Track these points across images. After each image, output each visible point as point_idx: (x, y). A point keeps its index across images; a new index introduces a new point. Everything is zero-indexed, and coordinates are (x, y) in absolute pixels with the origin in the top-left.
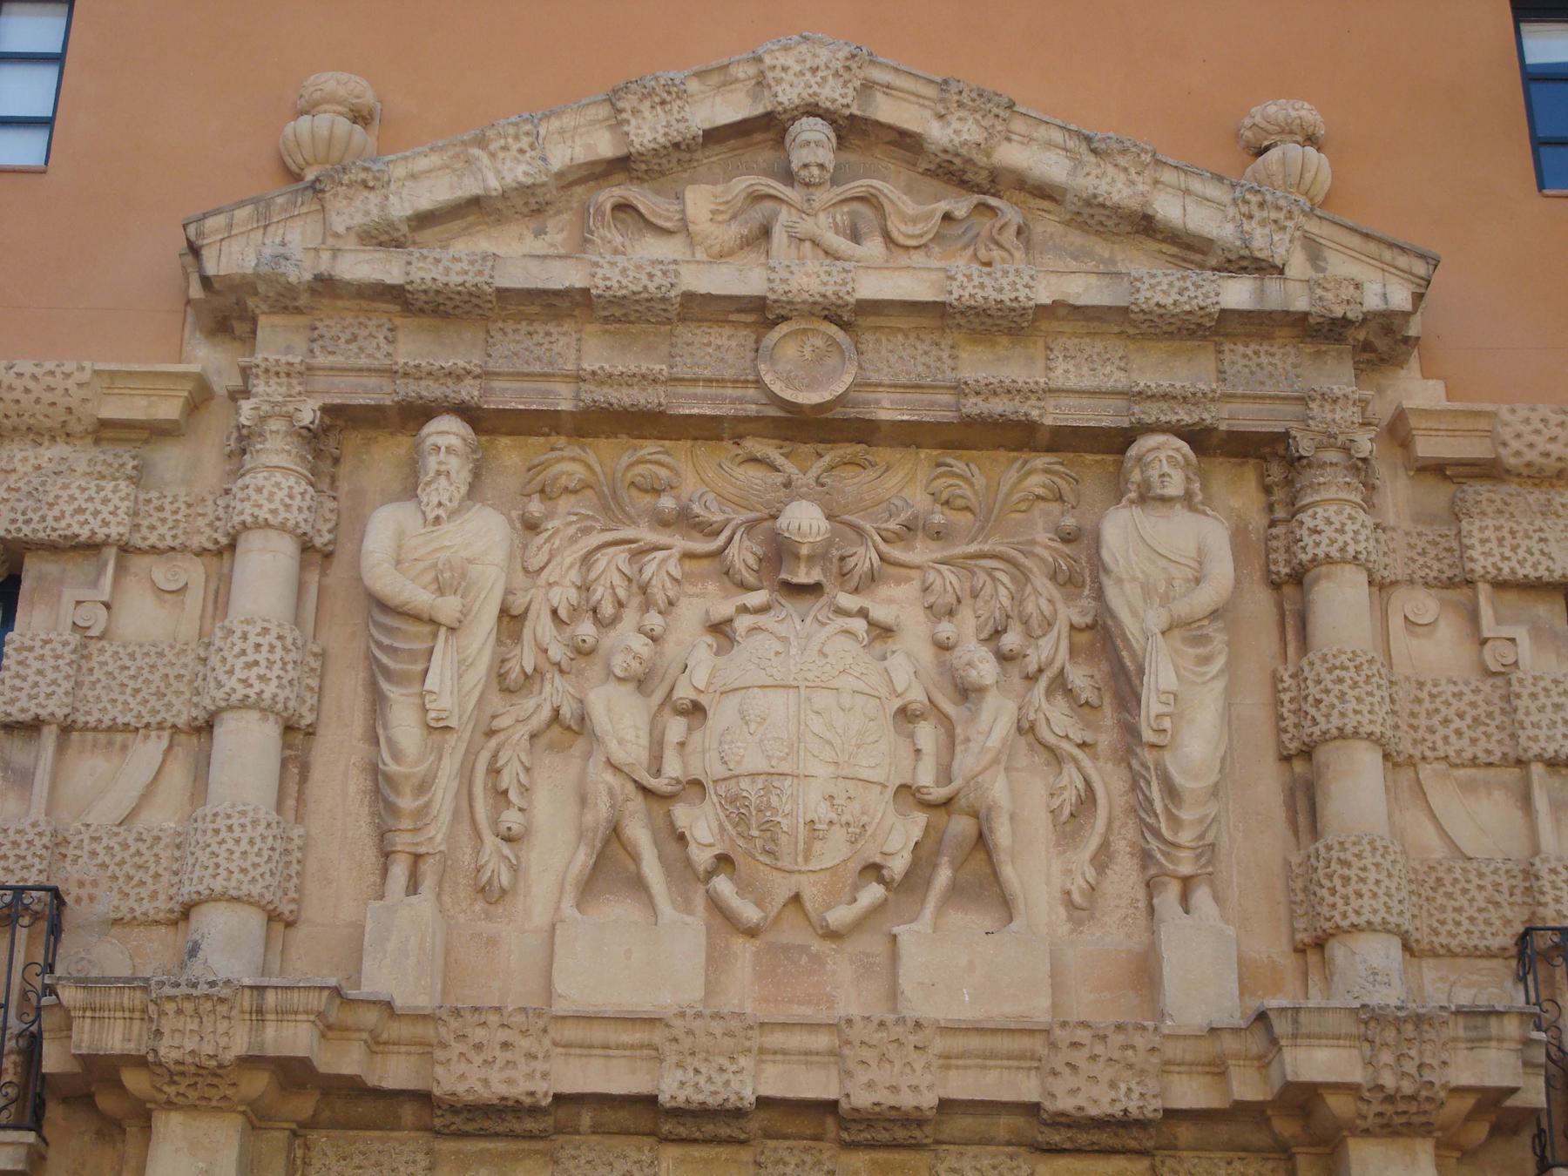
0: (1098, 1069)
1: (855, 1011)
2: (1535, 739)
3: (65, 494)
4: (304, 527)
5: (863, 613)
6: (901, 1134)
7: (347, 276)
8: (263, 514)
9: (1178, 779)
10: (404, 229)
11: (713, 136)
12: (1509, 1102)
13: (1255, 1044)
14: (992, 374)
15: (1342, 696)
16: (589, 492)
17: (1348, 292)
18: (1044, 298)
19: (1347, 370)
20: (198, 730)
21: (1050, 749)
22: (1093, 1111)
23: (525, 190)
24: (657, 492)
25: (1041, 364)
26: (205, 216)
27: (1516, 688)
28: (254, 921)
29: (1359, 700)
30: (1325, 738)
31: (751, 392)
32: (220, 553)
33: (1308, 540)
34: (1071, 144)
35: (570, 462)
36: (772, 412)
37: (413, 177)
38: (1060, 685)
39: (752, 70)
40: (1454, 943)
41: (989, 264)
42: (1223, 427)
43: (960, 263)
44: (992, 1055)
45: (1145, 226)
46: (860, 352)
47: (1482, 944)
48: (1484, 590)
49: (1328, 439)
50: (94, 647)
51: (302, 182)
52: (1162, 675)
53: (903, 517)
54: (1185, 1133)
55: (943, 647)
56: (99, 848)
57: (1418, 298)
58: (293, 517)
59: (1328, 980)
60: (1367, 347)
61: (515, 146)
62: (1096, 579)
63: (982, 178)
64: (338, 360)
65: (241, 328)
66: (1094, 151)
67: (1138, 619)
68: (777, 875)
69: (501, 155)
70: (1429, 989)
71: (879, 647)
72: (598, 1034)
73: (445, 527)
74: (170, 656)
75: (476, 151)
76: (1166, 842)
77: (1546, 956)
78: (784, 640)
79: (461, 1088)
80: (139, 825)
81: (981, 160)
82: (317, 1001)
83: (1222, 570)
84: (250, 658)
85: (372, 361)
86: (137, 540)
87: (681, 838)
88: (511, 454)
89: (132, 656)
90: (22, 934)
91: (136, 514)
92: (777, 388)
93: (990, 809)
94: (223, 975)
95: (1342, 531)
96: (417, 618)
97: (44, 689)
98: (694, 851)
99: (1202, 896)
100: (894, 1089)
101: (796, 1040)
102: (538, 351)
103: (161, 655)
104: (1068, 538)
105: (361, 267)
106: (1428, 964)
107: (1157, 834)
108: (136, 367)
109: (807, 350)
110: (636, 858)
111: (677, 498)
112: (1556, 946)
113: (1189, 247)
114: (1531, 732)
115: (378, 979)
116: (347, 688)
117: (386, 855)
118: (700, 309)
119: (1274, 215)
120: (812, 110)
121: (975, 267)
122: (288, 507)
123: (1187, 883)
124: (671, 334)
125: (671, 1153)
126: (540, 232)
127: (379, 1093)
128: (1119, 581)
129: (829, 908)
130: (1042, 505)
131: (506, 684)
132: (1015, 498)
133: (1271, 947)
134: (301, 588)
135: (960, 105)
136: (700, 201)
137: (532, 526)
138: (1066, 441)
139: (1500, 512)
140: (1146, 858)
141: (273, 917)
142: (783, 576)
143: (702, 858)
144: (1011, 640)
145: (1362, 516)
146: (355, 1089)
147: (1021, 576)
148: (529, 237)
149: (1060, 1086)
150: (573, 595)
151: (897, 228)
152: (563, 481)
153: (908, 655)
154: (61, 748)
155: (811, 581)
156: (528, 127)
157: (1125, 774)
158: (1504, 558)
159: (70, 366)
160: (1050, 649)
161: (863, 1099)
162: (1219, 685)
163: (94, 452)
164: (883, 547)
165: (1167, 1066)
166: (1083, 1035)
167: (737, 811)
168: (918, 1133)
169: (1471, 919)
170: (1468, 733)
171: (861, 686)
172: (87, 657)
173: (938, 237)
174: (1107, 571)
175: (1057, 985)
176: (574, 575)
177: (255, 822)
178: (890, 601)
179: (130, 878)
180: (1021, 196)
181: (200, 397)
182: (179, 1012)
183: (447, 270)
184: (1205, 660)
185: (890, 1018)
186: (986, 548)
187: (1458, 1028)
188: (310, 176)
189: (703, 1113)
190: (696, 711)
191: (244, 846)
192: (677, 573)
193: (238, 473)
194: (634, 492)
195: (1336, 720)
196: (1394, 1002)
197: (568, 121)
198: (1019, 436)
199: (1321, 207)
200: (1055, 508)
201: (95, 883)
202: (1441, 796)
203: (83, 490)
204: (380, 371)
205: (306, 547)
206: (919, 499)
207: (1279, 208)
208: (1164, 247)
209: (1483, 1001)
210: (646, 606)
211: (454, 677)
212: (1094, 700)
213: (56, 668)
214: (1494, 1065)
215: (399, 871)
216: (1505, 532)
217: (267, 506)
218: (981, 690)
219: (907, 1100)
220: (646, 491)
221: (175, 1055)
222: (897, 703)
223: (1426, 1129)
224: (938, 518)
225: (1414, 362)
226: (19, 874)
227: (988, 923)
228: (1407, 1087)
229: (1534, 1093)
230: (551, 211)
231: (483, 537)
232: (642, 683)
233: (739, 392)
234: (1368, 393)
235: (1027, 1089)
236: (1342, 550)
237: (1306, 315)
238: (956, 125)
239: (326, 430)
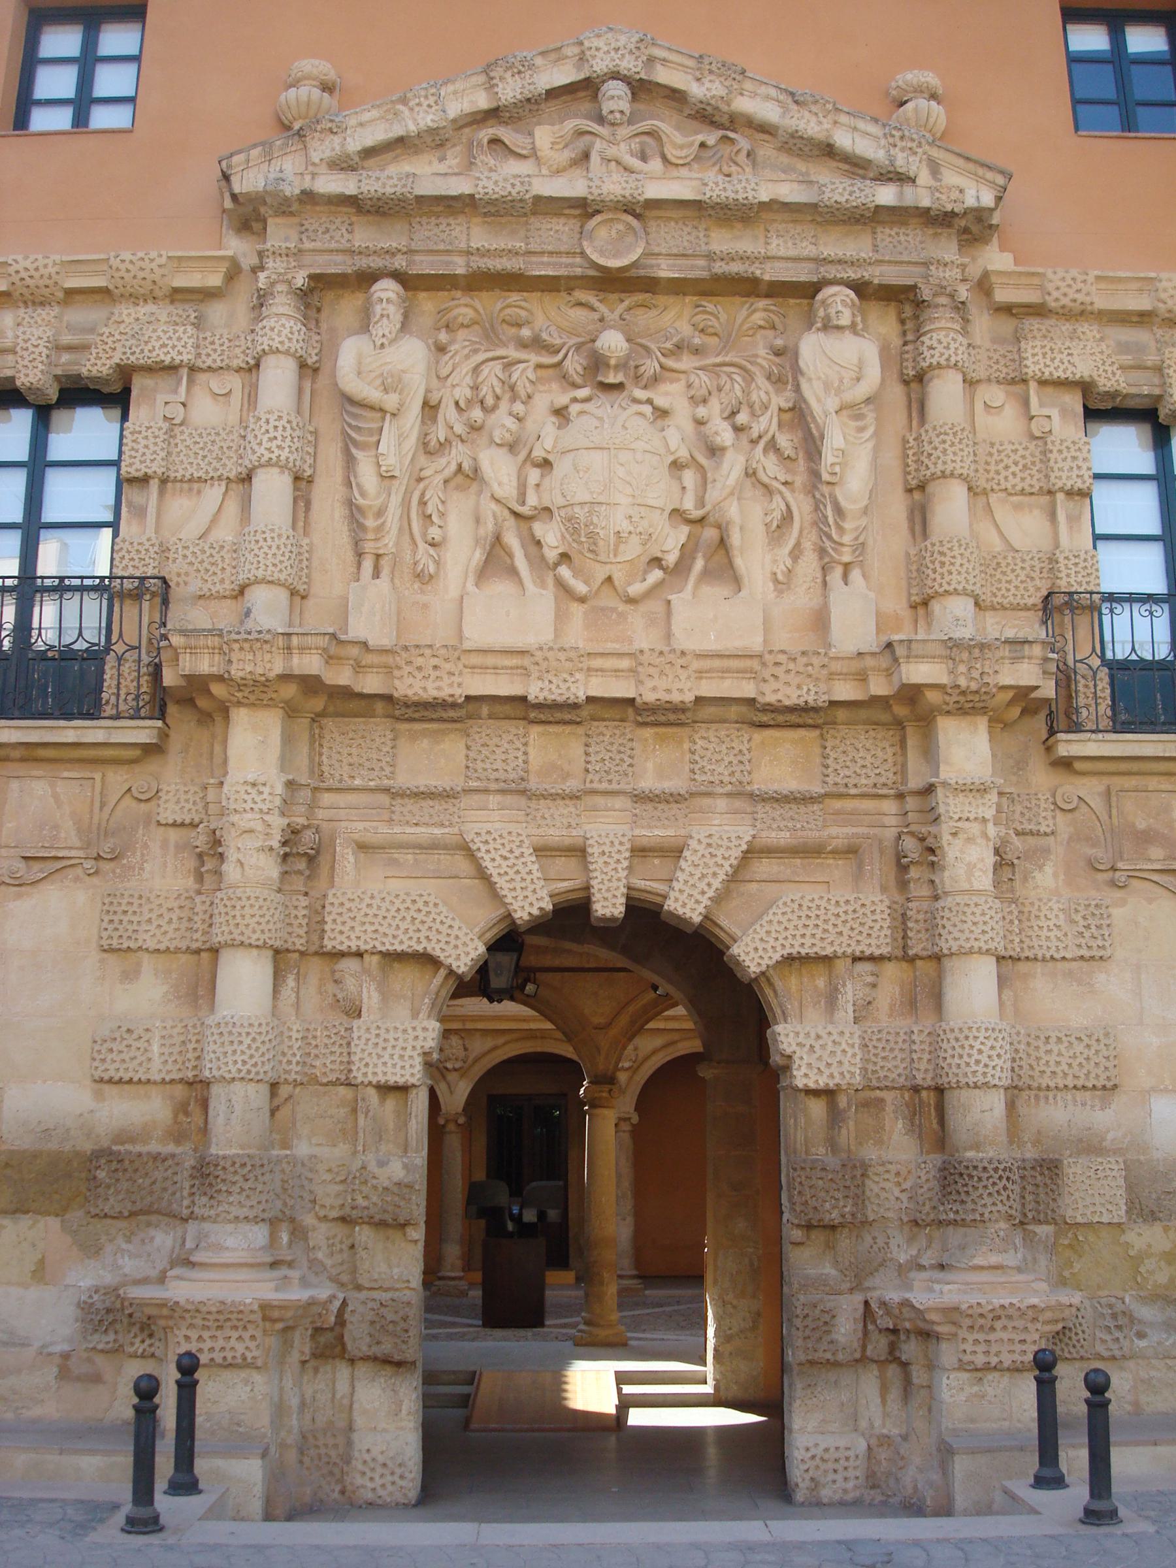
0: (790, 677)
1: (645, 646)
2: (1060, 478)
3: (154, 336)
4: (300, 352)
5: (649, 401)
6: (672, 717)
7: (321, 191)
8: (275, 345)
9: (843, 503)
10: (357, 159)
11: (552, 94)
12: (1033, 695)
13: (885, 661)
14: (732, 247)
15: (944, 451)
16: (476, 327)
17: (955, 195)
18: (764, 198)
19: (954, 246)
20: (243, 480)
21: (765, 486)
22: (787, 703)
23: (432, 131)
24: (519, 326)
25: (762, 240)
26: (232, 155)
27: (1050, 446)
28: (283, 595)
29: (955, 454)
30: (934, 477)
31: (578, 260)
32: (250, 370)
33: (927, 354)
34: (781, 97)
35: (464, 307)
36: (592, 273)
37: (361, 125)
38: (772, 446)
39: (576, 50)
40: (1005, 602)
41: (729, 176)
42: (876, 281)
43: (711, 175)
44: (728, 671)
45: (828, 151)
46: (647, 234)
47: (1022, 602)
48: (1033, 385)
49: (941, 290)
50: (177, 430)
51: (292, 130)
52: (835, 438)
53: (675, 340)
54: (841, 714)
55: (700, 423)
56: (188, 553)
57: (999, 199)
58: (294, 346)
59: (929, 624)
60: (966, 231)
61: (425, 103)
62: (795, 379)
63: (725, 120)
64: (318, 245)
65: (256, 226)
66: (796, 102)
67: (821, 403)
68: (598, 565)
69: (417, 109)
70: (989, 629)
71: (659, 423)
72: (490, 660)
73: (387, 350)
74: (223, 434)
75: (400, 107)
76: (835, 542)
77: (1059, 610)
78: (600, 419)
79: (410, 693)
80: (211, 538)
81: (725, 108)
82: (323, 642)
83: (874, 373)
84: (272, 435)
85: (338, 245)
86: (199, 363)
87: (539, 543)
88: (427, 303)
89: (201, 435)
90: (146, 605)
91: (198, 347)
92: (594, 257)
93: (728, 523)
94: (266, 627)
95: (947, 348)
96: (372, 408)
97: (149, 457)
98: (546, 550)
99: (856, 574)
100: (668, 691)
101: (609, 663)
102: (443, 236)
103: (218, 434)
104: (778, 353)
105: (331, 184)
106: (989, 614)
107: (830, 537)
108: (193, 254)
109: (614, 232)
110: (510, 555)
111: (532, 329)
112: (1066, 603)
113: (855, 165)
114: (1057, 474)
115: (358, 629)
116: (331, 453)
117: (360, 555)
118: (545, 206)
119: (909, 145)
120: (615, 76)
121: (720, 178)
122: (290, 339)
123: (847, 567)
124: (527, 223)
125: (535, 730)
126: (442, 159)
127: (361, 696)
128: (810, 380)
129: (629, 584)
130: (763, 332)
131: (429, 448)
132: (745, 327)
133: (896, 604)
134: (300, 391)
135: (711, 72)
136: (544, 136)
138: (779, 290)
139: (1045, 337)
140: (822, 552)
141: (293, 593)
142: (600, 378)
143: (551, 555)
144: (742, 418)
145: (960, 338)
146: (347, 693)
147: (749, 377)
148: (435, 162)
149: (767, 688)
150: (468, 393)
151: (670, 152)
152: (460, 320)
153: (678, 427)
154: (162, 493)
155: (616, 381)
156: (433, 90)
157: (811, 501)
158: (1047, 366)
159: (153, 254)
160: (766, 423)
161: (650, 697)
162: (870, 445)
163: (171, 308)
164: (662, 359)
165: (831, 676)
166: (782, 658)
167: (572, 526)
168: (682, 717)
169: (1016, 587)
170: (1020, 475)
171: (648, 447)
172: (174, 437)
173: (697, 158)
174: (802, 374)
175: (767, 631)
176: (468, 380)
177: (280, 536)
178: (667, 394)
179: (207, 570)
180: (748, 132)
181: (233, 272)
182: (241, 649)
183: (384, 185)
184: (861, 429)
185: (666, 649)
186: (727, 359)
187: (1006, 651)
188: (296, 126)
189: (555, 706)
190: (546, 464)
191: (274, 550)
192: (532, 377)
193: (259, 319)
194: (505, 326)
195: (940, 467)
196: (968, 636)
197: (459, 85)
198: (748, 287)
199: (941, 140)
200: (770, 333)
201: (187, 574)
202: (1002, 513)
203: (165, 332)
204: (344, 251)
205: (303, 365)
206: (685, 329)
207: (913, 140)
208: (841, 165)
209: (1021, 635)
210: (514, 399)
211: (396, 444)
212: (793, 455)
213: (156, 444)
214: (1026, 673)
215: (368, 564)
216: (1047, 349)
217: (277, 339)
218: (723, 449)
219: (676, 697)
220: (512, 325)
221: (241, 674)
222: (671, 458)
223: (984, 710)
224: (697, 341)
225: (995, 240)
226: (142, 569)
227: (726, 593)
228: (974, 686)
229: (1048, 690)
230: (449, 145)
231: (410, 356)
232: (512, 447)
233: (570, 260)
234: (966, 260)
235: (747, 690)
236: (948, 360)
237: (929, 209)
238: (708, 85)
239: (312, 290)
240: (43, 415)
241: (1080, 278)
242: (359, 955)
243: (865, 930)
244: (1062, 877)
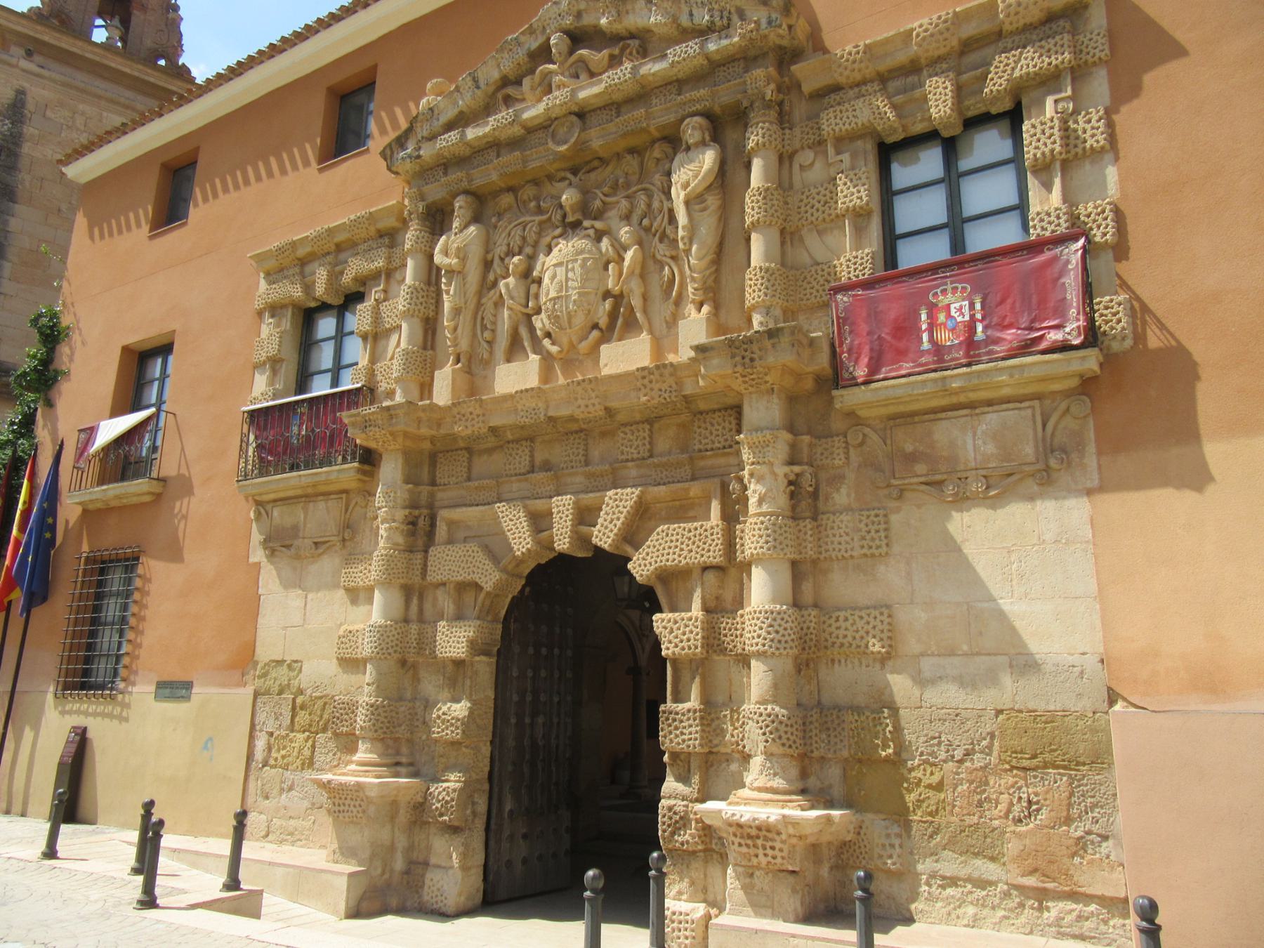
240: (951, 148)
242: (444, 584)
243: (706, 547)
244: (853, 495)
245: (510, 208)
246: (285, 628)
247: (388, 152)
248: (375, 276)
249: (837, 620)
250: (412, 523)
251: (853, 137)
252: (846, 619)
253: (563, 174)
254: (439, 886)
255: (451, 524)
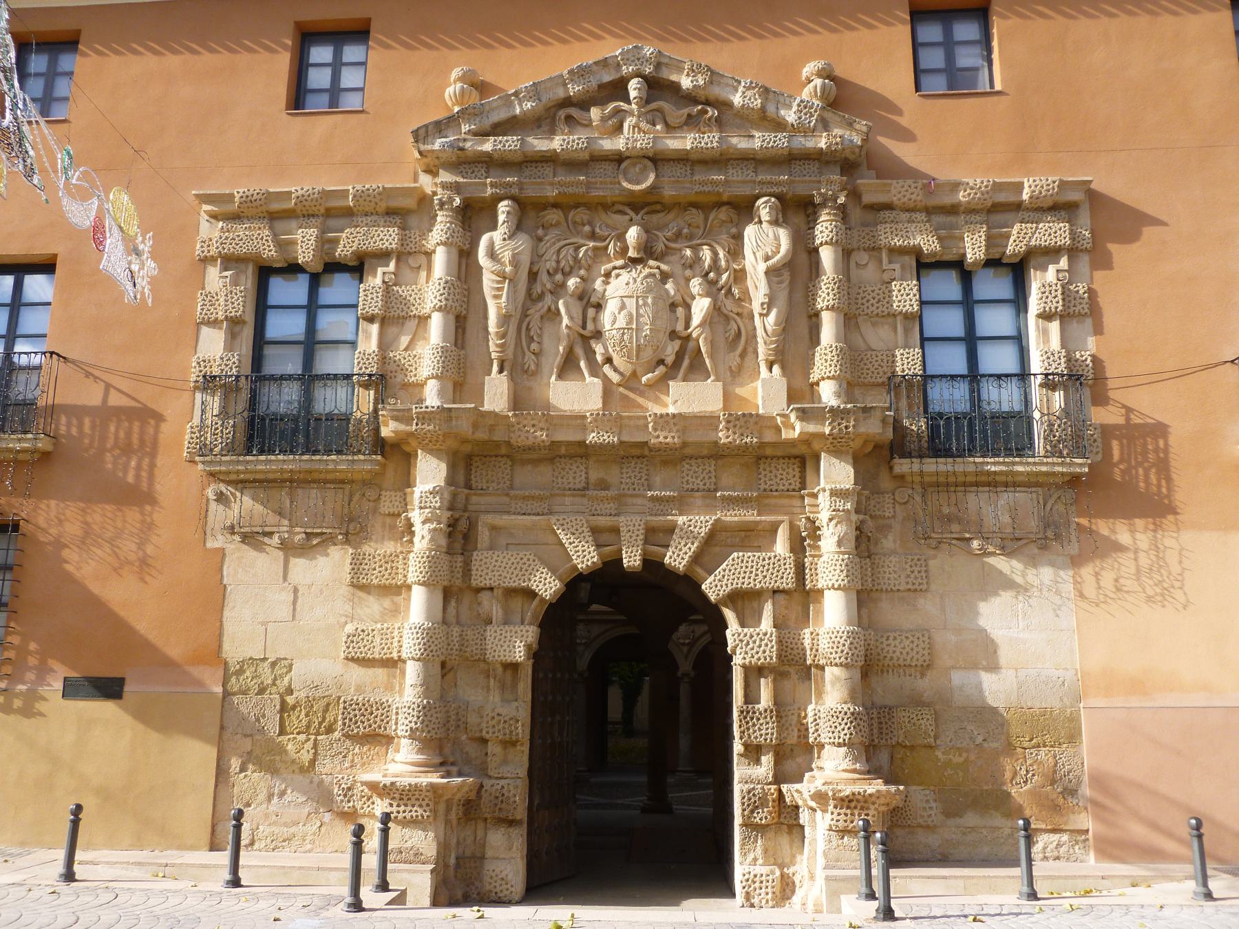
5: (658, 268)
136: (595, 113)
137: (540, 240)
150: (554, 264)
184: (780, 282)
240: (315, 281)
241: (913, 185)
242: (491, 589)
245: (558, 224)
246: (264, 623)
247: (422, 132)
248: (383, 256)
249: (888, 639)
250: (453, 524)
251: (903, 251)
252: (895, 638)
253: (621, 207)
254: (503, 875)
255: (494, 528)
